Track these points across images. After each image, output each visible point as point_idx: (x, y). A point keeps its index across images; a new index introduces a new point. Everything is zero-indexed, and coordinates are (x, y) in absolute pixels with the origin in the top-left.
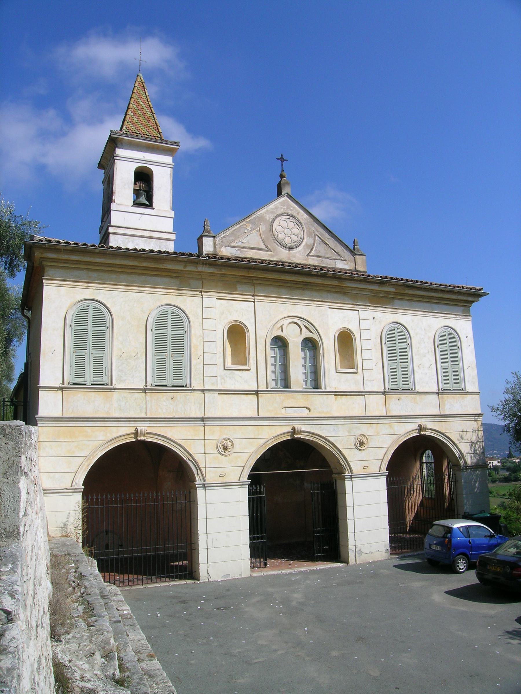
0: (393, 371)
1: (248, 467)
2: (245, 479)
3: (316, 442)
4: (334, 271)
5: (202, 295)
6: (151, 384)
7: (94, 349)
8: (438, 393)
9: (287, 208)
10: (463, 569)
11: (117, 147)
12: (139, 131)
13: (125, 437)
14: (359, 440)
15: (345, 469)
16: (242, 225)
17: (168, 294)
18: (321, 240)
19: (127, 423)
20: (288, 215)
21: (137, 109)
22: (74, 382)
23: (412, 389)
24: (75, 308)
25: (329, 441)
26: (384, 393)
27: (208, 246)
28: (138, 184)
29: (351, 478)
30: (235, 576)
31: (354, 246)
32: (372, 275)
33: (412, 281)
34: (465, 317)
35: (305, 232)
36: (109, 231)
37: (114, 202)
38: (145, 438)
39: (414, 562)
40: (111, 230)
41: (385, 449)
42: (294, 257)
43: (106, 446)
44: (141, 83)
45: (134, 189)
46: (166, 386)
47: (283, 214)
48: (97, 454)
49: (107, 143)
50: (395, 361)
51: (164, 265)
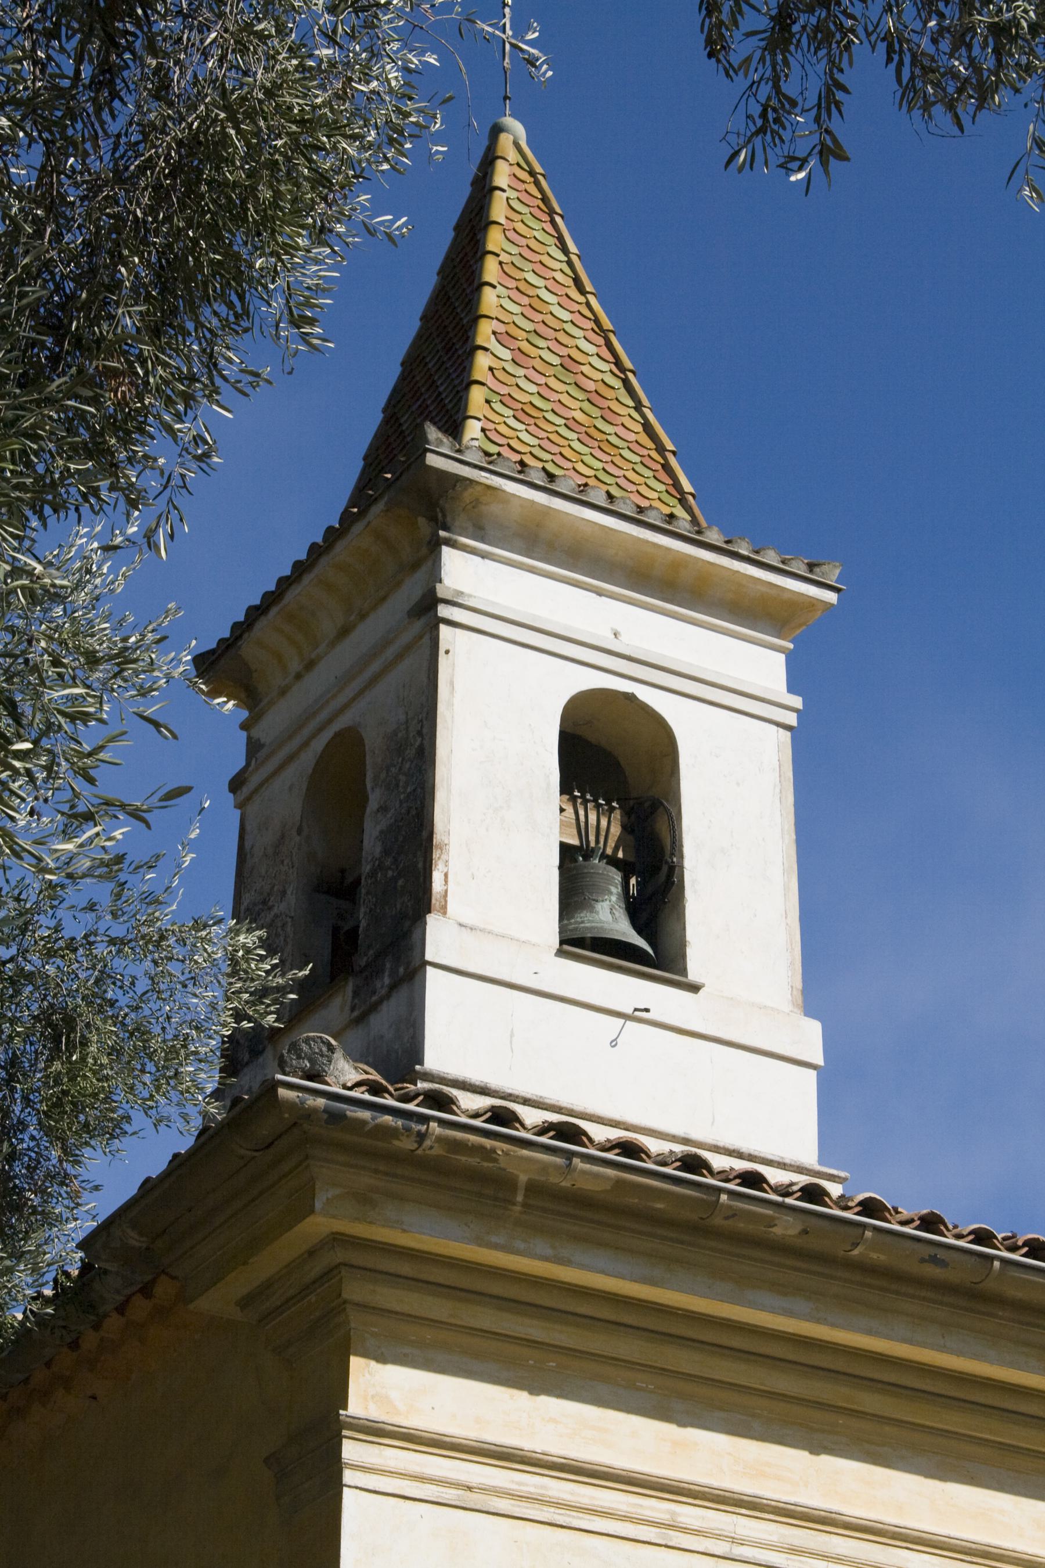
21: (528, 326)
37: (444, 910)
44: (524, 175)
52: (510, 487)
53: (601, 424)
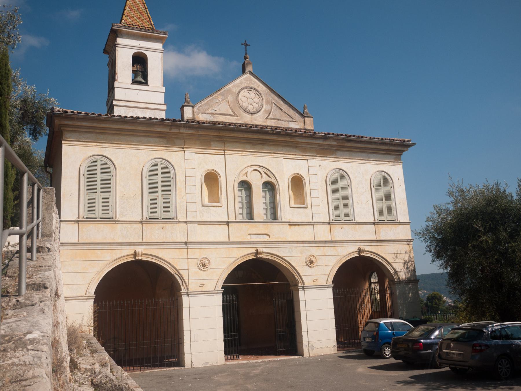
0: (337, 207)
1: (221, 279)
2: (219, 288)
3: (275, 261)
4: (286, 130)
5: (184, 151)
6: (146, 218)
7: (102, 192)
8: (374, 223)
9: (249, 83)
10: (388, 355)
11: (118, 37)
12: (135, 23)
13: (127, 257)
14: (309, 259)
15: (298, 281)
16: (215, 97)
17: (158, 150)
18: (277, 106)
19: (128, 247)
20: (250, 88)
21: (133, 5)
22: (87, 217)
23: (352, 220)
24: (87, 161)
25: (285, 260)
26: (329, 223)
27: (188, 113)
28: (136, 66)
29: (304, 289)
30: (212, 364)
31: (304, 110)
32: (317, 132)
33: (350, 136)
34: (396, 163)
35: (264, 100)
36: (113, 104)
37: (117, 81)
38: (142, 258)
39: (356, 354)
40: (115, 103)
41: (331, 267)
42: (256, 120)
43: (112, 264)
45: (132, 70)
46: (158, 219)
47: (246, 87)
48: (105, 270)
49: (110, 34)
50: (338, 198)
51: (154, 128)
52: (123, 29)
53: (142, 17)
